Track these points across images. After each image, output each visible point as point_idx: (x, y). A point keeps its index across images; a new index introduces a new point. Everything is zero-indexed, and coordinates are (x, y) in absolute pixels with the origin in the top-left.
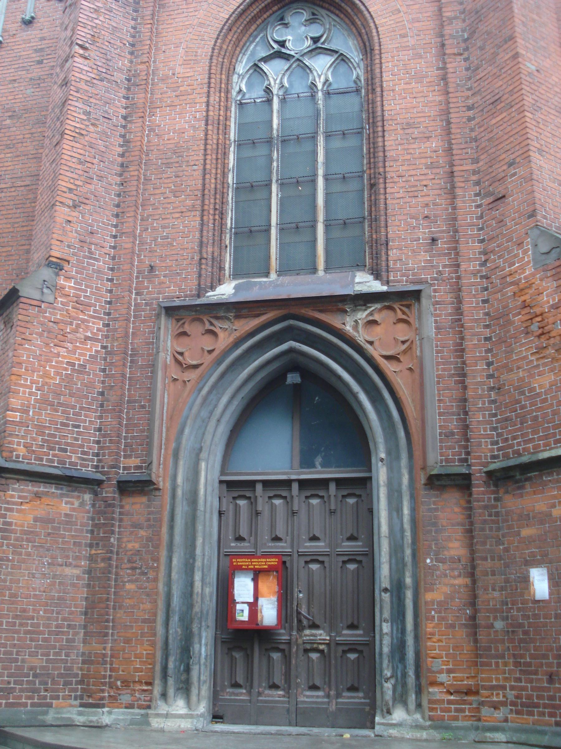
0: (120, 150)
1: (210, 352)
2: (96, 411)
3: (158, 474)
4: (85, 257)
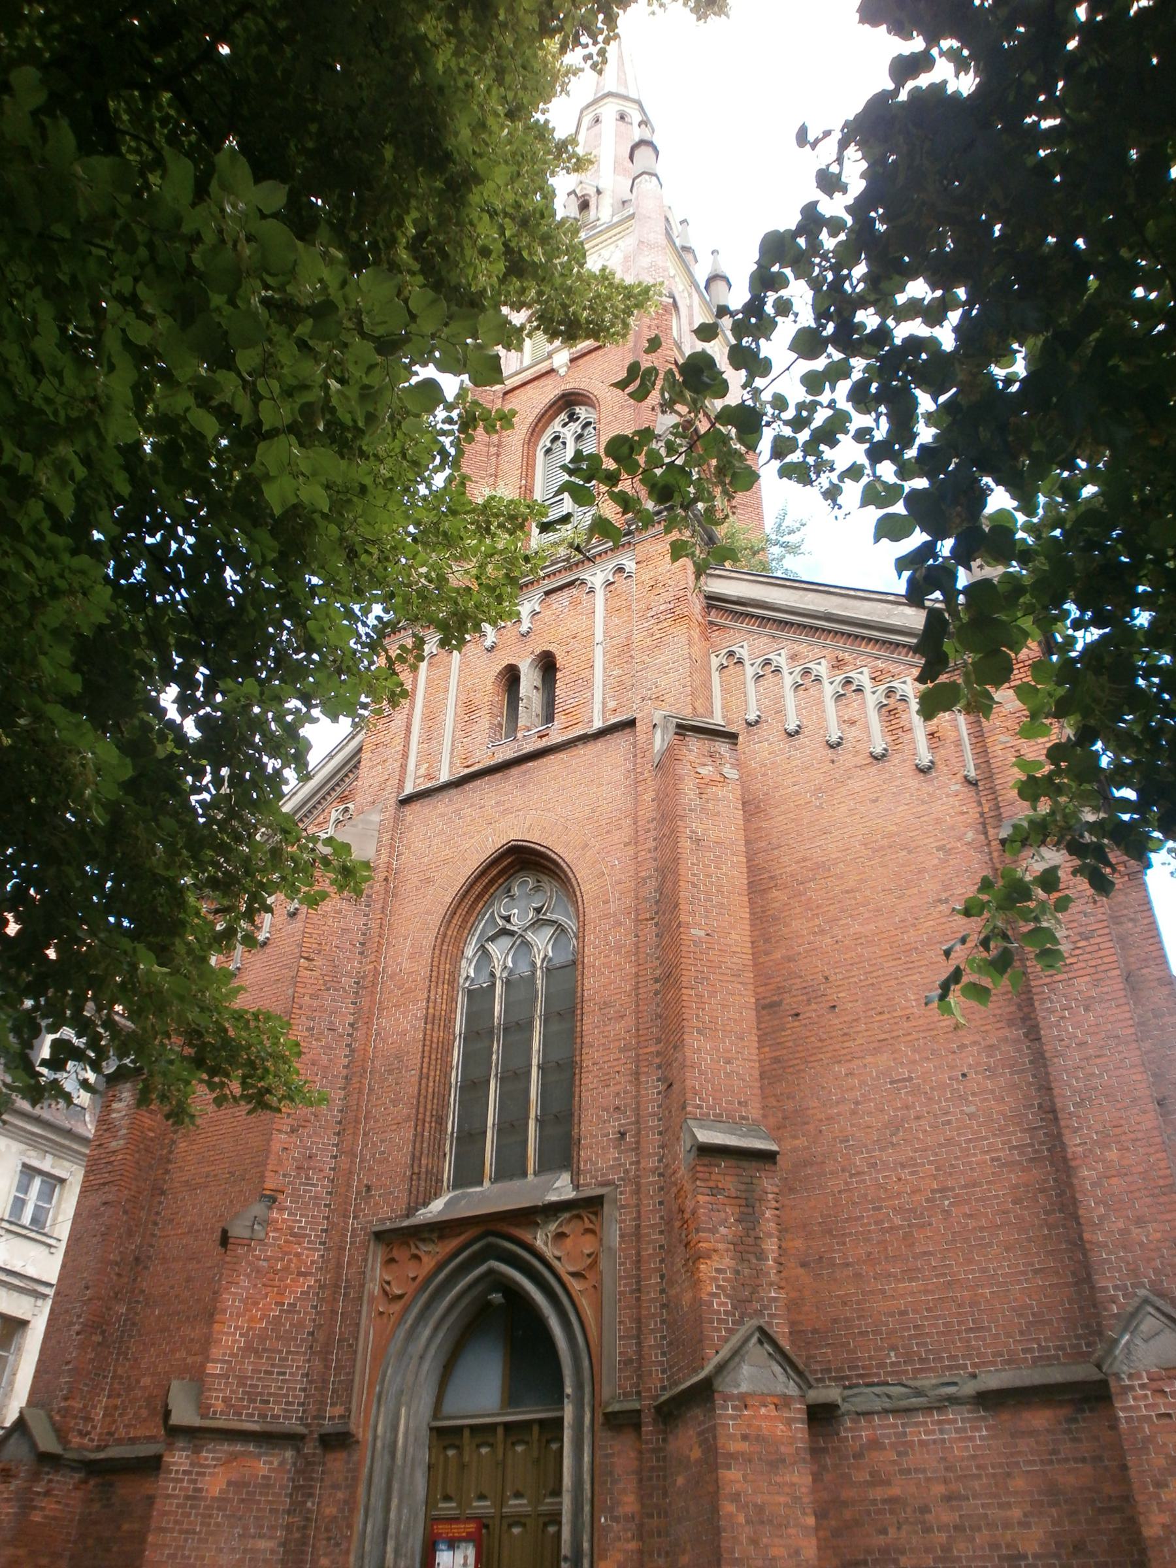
0: (346, 1061)
1: (414, 1279)
2: (305, 1353)
3: (356, 1427)
4: (301, 1184)
